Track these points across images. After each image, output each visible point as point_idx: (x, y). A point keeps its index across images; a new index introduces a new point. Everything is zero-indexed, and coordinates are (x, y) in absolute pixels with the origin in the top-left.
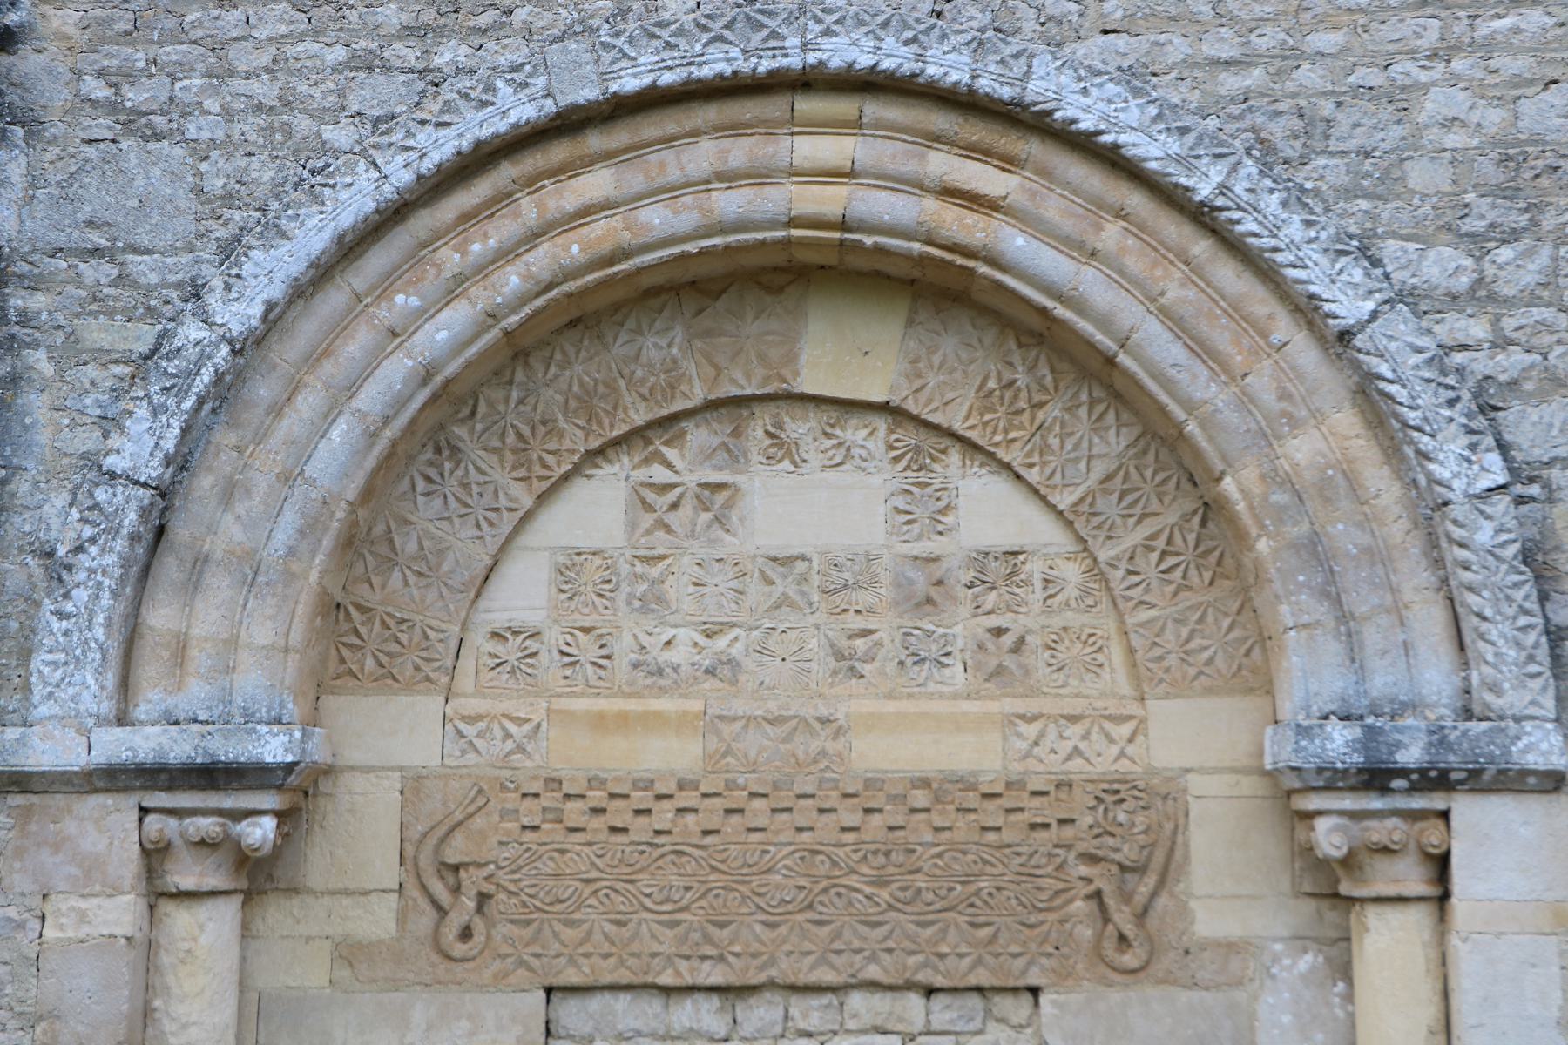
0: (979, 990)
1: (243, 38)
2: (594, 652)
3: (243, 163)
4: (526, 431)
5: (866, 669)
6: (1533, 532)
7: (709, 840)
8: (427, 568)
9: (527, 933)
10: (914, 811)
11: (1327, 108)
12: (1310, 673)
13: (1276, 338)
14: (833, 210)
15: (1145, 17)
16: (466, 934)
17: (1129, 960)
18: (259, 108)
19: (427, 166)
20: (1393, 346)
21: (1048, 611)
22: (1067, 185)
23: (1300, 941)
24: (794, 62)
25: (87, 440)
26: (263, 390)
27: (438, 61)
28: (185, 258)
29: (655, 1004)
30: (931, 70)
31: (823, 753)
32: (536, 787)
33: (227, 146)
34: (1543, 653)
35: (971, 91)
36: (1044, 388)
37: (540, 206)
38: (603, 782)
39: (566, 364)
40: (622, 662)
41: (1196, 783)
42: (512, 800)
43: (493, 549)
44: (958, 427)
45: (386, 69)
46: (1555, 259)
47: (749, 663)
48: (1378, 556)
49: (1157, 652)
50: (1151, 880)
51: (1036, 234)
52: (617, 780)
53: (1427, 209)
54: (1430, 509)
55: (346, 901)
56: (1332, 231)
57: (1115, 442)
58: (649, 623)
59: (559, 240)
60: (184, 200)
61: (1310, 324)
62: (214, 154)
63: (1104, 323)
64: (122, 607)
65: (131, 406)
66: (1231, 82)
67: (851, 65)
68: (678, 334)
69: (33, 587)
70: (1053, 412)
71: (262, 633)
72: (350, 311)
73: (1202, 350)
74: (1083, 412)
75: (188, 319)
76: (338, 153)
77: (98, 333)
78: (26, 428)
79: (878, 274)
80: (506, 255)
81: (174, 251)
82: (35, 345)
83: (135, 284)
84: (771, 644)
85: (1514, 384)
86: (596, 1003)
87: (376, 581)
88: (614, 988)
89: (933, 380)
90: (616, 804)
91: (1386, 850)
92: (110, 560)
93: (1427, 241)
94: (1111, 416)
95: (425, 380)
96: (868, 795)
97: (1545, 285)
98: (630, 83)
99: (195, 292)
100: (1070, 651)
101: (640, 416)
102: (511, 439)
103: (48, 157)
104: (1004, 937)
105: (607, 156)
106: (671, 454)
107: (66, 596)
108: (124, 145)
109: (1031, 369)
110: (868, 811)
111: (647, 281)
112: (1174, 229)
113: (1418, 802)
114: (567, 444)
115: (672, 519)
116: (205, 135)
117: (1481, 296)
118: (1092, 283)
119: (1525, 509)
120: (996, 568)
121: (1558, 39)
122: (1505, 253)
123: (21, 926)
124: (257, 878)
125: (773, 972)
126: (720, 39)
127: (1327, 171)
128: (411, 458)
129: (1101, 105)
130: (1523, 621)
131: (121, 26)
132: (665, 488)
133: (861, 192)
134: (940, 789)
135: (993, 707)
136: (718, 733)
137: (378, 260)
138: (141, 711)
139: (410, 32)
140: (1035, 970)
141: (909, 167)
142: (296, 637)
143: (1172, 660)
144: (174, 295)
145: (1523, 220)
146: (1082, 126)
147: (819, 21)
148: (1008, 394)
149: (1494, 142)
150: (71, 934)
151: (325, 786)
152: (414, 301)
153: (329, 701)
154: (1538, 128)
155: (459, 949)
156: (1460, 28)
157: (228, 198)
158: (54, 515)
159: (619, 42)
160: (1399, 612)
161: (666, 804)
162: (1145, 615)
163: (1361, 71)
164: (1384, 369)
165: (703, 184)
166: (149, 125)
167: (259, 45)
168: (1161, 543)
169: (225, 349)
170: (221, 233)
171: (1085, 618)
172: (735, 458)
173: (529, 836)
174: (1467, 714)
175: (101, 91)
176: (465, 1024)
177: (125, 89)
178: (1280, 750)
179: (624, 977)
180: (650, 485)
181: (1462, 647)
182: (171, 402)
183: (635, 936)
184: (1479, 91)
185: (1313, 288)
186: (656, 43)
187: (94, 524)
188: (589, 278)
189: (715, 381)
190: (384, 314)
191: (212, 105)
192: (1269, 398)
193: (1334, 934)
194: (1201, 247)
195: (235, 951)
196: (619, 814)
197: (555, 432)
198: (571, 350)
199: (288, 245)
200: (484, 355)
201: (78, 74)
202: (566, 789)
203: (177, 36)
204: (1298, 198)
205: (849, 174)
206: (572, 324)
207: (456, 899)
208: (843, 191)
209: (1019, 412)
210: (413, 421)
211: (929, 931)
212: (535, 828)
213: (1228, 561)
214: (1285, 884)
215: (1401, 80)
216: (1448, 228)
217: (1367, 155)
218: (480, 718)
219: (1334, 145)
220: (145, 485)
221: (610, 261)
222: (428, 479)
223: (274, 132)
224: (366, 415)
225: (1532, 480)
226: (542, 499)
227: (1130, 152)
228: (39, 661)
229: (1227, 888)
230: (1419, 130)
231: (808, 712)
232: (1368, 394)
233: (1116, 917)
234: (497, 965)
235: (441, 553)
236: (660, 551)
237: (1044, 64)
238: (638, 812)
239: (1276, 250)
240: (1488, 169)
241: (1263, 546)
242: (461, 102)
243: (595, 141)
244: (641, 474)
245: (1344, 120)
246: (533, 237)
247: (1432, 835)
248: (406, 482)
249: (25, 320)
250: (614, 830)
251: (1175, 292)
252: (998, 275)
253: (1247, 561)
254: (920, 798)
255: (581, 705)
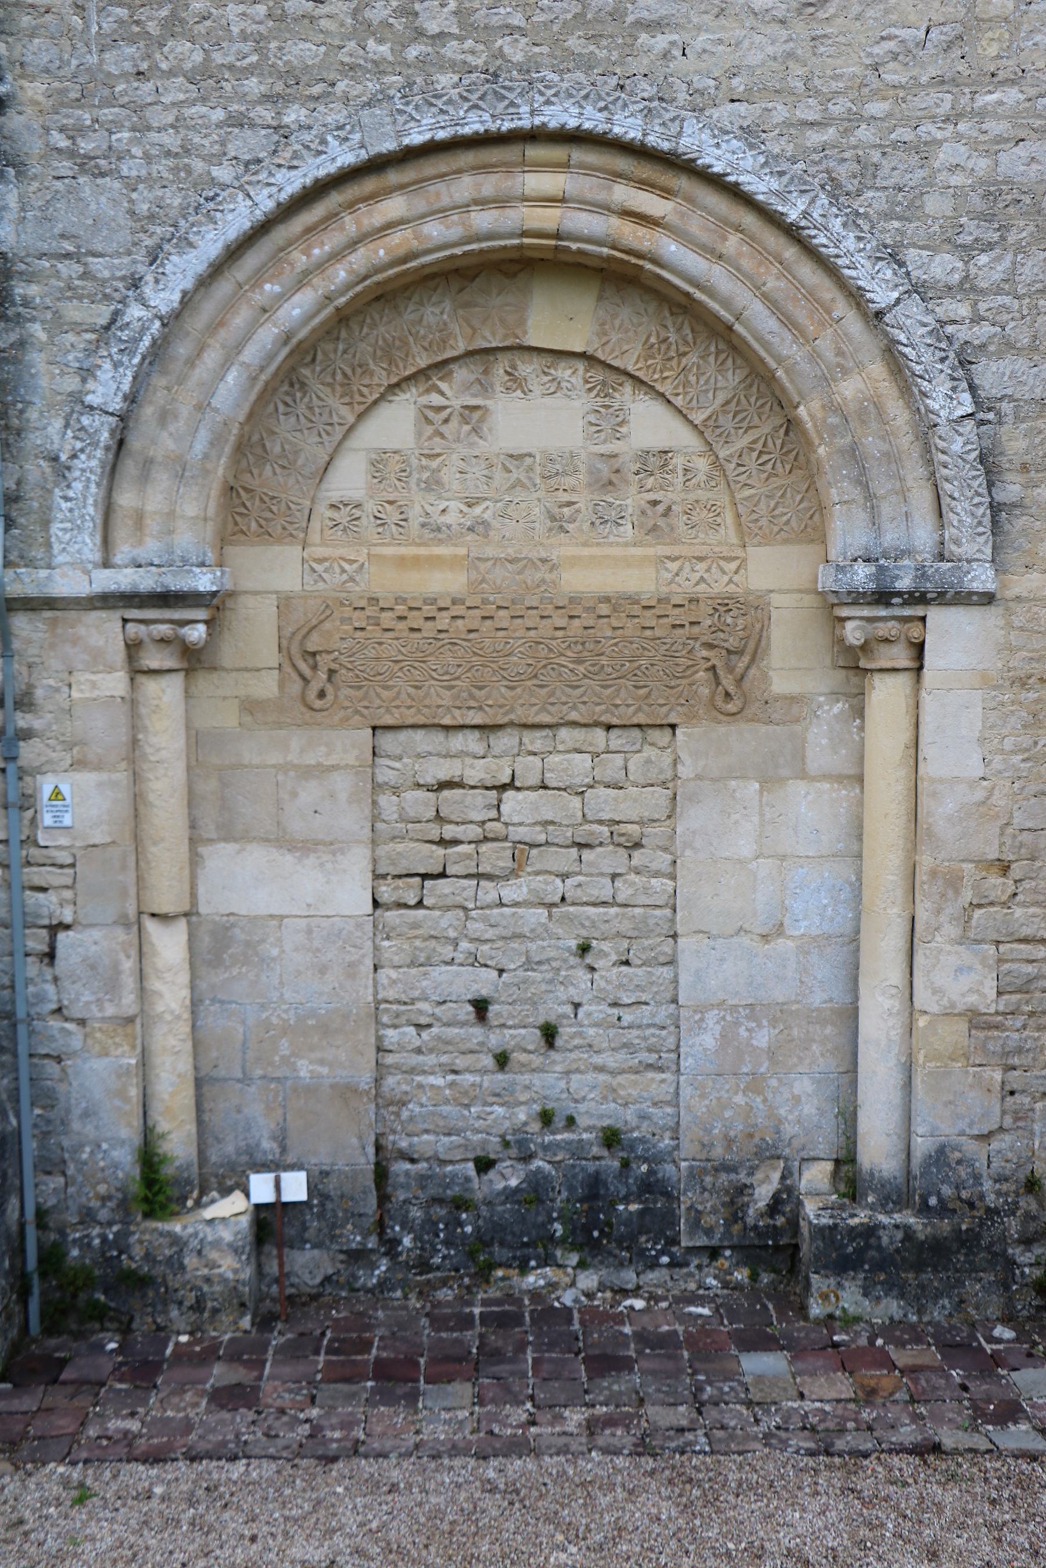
0: (639, 726)
1: (155, 103)
2: (396, 517)
3: (160, 193)
4: (349, 372)
5: (570, 527)
6: (987, 443)
7: (472, 636)
8: (288, 463)
9: (360, 694)
10: (600, 617)
11: (876, 156)
12: (848, 532)
13: (836, 314)
14: (551, 226)
15: (759, 90)
16: (322, 694)
17: (731, 707)
18: (168, 154)
19: (284, 196)
20: (909, 322)
21: (686, 489)
22: (704, 208)
23: (835, 695)
24: (525, 123)
25: (71, 383)
26: (182, 349)
27: (286, 120)
28: (126, 260)
29: (439, 737)
30: (617, 130)
31: (543, 581)
32: (363, 603)
33: (149, 180)
34: (987, 520)
35: (643, 144)
36: (687, 343)
37: (358, 222)
38: (405, 600)
39: (374, 326)
40: (414, 524)
41: (776, 599)
42: (347, 611)
43: (330, 450)
44: (630, 368)
45: (252, 126)
46: (1014, 263)
47: (495, 524)
48: (892, 458)
49: (754, 516)
50: (746, 659)
51: (684, 245)
52: (414, 598)
53: (936, 228)
54: (925, 428)
55: (247, 675)
56: (874, 243)
57: (732, 379)
58: (431, 498)
59: (371, 246)
60: (123, 219)
61: (858, 304)
62: (141, 186)
63: (726, 304)
64: (102, 493)
65: (99, 362)
66: (815, 138)
67: (563, 126)
68: (447, 305)
69: (46, 480)
70: (692, 358)
71: (190, 509)
72: (235, 294)
73: (788, 322)
74: (712, 359)
75: (133, 304)
76: (224, 187)
77: (73, 311)
78: (32, 376)
79: (579, 265)
80: (336, 256)
81: (119, 255)
82: (33, 320)
83: (94, 278)
84: (509, 511)
85: (983, 346)
86: (403, 736)
87: (255, 471)
88: (414, 726)
89: (614, 337)
90: (413, 614)
91: (887, 640)
92: (94, 463)
93: (935, 250)
94: (730, 361)
95: (285, 343)
96: (571, 607)
97: (1006, 281)
98: (416, 138)
99: (135, 283)
100: (701, 515)
101: (423, 362)
102: (339, 377)
103: (31, 189)
104: (655, 694)
105: (401, 187)
106: (443, 386)
107: (69, 486)
108: (81, 180)
109: (679, 330)
110: (571, 617)
111: (427, 271)
112: (773, 240)
113: (907, 612)
114: (376, 380)
115: (444, 429)
116: (134, 173)
117: (967, 288)
118: (718, 276)
119: (983, 428)
120: (654, 462)
121: (1026, 110)
122: (983, 259)
123: (57, 690)
124: (193, 660)
125: (512, 717)
126: (476, 107)
127: (874, 200)
128: (275, 390)
129: (728, 155)
130: (977, 500)
131: (73, 95)
132: (440, 409)
133: (571, 214)
134: (618, 603)
135: (650, 551)
136: (477, 568)
137: (252, 260)
138: (118, 559)
139: (267, 98)
140: (673, 714)
141: (601, 196)
142: (211, 511)
143: (764, 522)
144: (120, 285)
145: (996, 236)
146: (715, 170)
147: (542, 94)
148: (663, 347)
149: (982, 182)
150: (87, 695)
151: (229, 604)
152: (277, 288)
153: (229, 550)
154: (1010, 173)
155: (318, 704)
156: (964, 100)
157: (152, 217)
158: (48, 430)
159: (409, 109)
160: (903, 493)
161: (444, 614)
162: (748, 492)
163: (900, 130)
164: (902, 338)
165: (465, 207)
166: (97, 166)
167: (166, 108)
168: (759, 446)
169: (157, 324)
170: (148, 242)
171: (709, 494)
172: (485, 388)
173: (359, 634)
174: (941, 557)
175: (64, 143)
176: (323, 749)
177: (79, 140)
178: (827, 580)
179: (421, 720)
180: (431, 407)
181: (941, 516)
182: (125, 359)
183: (427, 694)
184: (974, 145)
185: (860, 283)
186: (434, 109)
187: (82, 440)
188: (391, 272)
189: (473, 336)
190: (257, 298)
191: (137, 151)
192: (829, 355)
193: (855, 691)
194: (790, 252)
195: (182, 707)
196: (416, 620)
197: (367, 372)
198: (377, 317)
199: (194, 252)
200: (322, 324)
201: (47, 130)
202: (382, 604)
203: (109, 102)
204: (852, 221)
205: (560, 200)
206: (378, 299)
207: (316, 672)
208: (557, 212)
209: (670, 359)
210: (279, 368)
211: (609, 691)
212: (362, 629)
213: (801, 458)
214: (828, 661)
215: (925, 137)
216: (949, 241)
217: (900, 190)
218: (325, 560)
219: (879, 183)
220: (112, 414)
221: (404, 260)
222: (286, 404)
223: (179, 170)
224: (248, 366)
225: (990, 409)
226: (361, 417)
227: (746, 188)
228: (55, 528)
229: (793, 664)
230: (935, 172)
231: (534, 555)
232: (891, 353)
233: (724, 682)
234: (342, 713)
235: (296, 453)
236: (438, 451)
237: (691, 126)
238: (427, 619)
239: (838, 256)
240: (976, 201)
241: (822, 450)
242: (304, 152)
243: (393, 177)
244: (424, 400)
245: (886, 164)
246: (353, 244)
247: (915, 632)
248: (271, 407)
249: (26, 303)
250: (412, 630)
251: (772, 284)
252: (658, 271)
253: (813, 458)
254: (604, 609)
255: (389, 551)
